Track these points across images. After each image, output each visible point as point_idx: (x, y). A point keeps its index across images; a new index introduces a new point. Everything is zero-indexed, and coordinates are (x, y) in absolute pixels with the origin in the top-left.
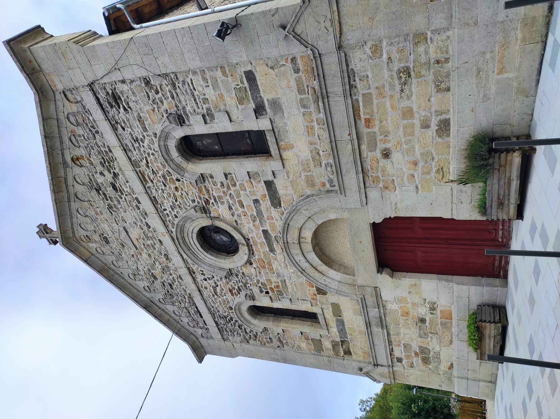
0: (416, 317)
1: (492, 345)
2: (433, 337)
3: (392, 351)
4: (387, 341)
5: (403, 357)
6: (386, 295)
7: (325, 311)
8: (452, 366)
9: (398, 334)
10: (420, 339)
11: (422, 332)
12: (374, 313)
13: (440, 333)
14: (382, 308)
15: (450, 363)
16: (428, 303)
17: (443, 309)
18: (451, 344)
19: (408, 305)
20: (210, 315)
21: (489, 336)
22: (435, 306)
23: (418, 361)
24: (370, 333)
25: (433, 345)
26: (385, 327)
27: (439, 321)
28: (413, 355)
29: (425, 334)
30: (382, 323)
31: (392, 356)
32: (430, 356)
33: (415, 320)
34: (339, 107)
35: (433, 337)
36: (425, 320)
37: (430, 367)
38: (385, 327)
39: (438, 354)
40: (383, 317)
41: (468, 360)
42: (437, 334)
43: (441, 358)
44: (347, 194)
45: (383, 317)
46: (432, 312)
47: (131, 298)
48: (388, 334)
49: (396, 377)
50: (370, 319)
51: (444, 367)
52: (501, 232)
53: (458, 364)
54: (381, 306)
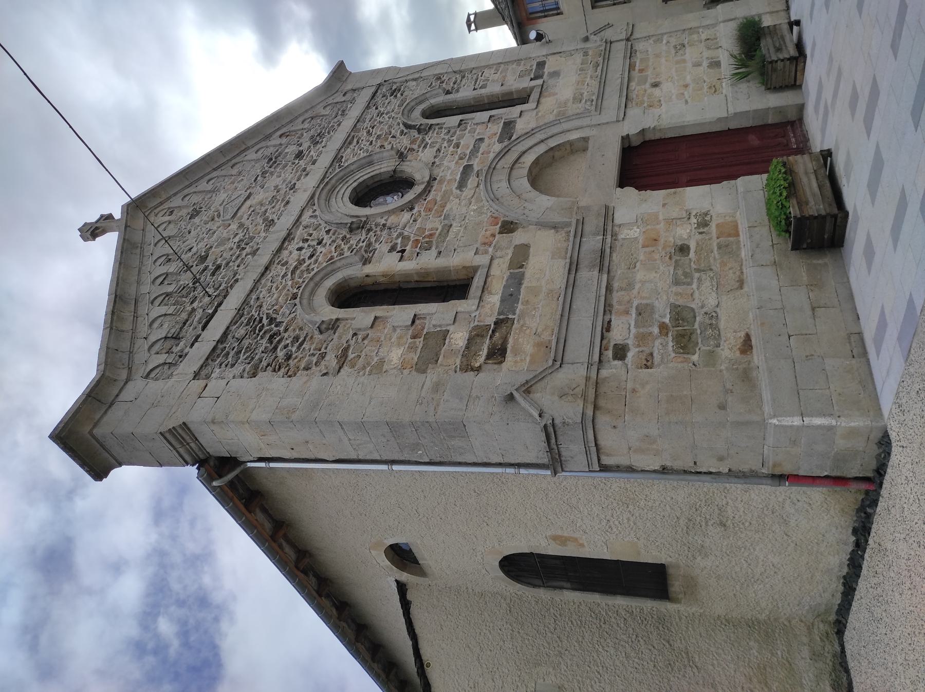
0: (671, 244)
1: (815, 184)
2: (704, 277)
3: (608, 330)
4: (603, 299)
5: (630, 342)
6: (621, 216)
7: (496, 262)
8: (747, 345)
9: (630, 286)
10: (674, 289)
11: (680, 272)
12: (592, 243)
13: (716, 267)
14: (609, 237)
15: (742, 334)
16: (696, 216)
17: (721, 221)
18: (741, 287)
19: (658, 227)
20: (234, 312)
21: (806, 173)
22: (708, 218)
23: (663, 347)
24: (571, 281)
25: (704, 296)
26: (606, 269)
27: (715, 244)
28: (656, 330)
29: (686, 275)
30: (602, 262)
31: (604, 342)
32: (696, 326)
33: (668, 249)
34: (572, 276)
35: (704, 277)
36: (688, 248)
37: (695, 358)
38: (606, 269)
39: (713, 316)
40: (608, 250)
41: (783, 308)
42: (711, 270)
43: (722, 325)
44: (603, 113)
45: (608, 250)
46: (702, 230)
47: (118, 278)
48: (609, 289)
49: (602, 402)
50: (582, 255)
51: (728, 351)
52: (793, 140)
53: (762, 324)
54: (609, 233)
